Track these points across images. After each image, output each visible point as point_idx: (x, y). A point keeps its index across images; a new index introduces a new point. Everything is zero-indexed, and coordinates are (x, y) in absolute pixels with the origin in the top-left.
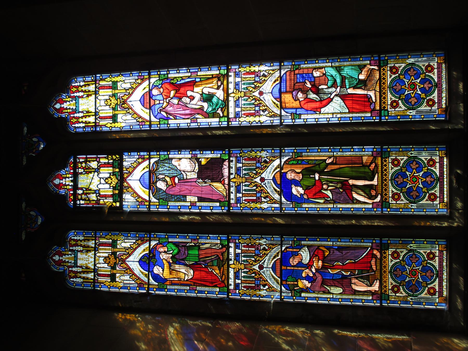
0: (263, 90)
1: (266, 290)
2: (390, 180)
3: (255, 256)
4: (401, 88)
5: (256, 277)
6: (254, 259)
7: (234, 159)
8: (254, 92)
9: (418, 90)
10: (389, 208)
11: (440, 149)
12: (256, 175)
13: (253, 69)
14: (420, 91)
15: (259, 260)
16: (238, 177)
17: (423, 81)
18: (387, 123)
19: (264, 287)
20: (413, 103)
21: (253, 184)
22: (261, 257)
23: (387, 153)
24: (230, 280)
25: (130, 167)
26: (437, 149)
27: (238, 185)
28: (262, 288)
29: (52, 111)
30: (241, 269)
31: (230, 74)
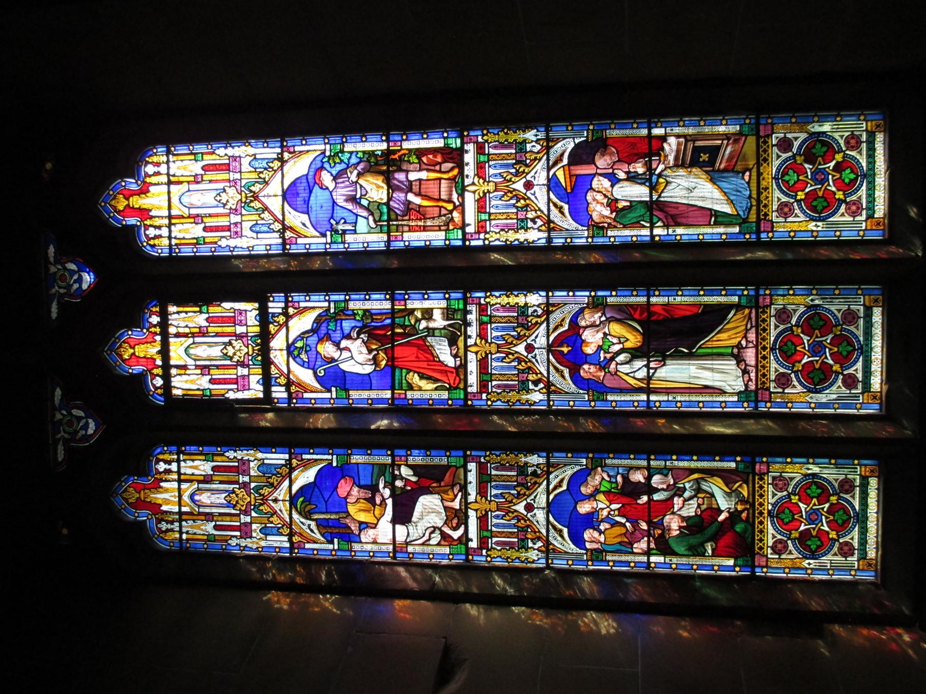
0: (532, 179)
1: (538, 549)
2: (774, 178)
3: (517, 486)
4: (798, 180)
5: (520, 367)
6: (515, 333)
7: (474, 309)
8: (515, 345)
9: (825, 524)
10: (770, 401)
11: (865, 292)
12: (516, 176)
13: (513, 300)
14: (829, 527)
15: (524, 172)
16: (481, 181)
17: (836, 341)
18: (771, 245)
19: (536, 385)
20: (818, 146)
21: (510, 356)
22: (528, 489)
23: (769, 127)
24: (469, 377)
25: (266, 169)
26: (860, 292)
27: (483, 516)
28: (531, 386)
29: (118, 501)
30: (489, 192)
31: (466, 147)
